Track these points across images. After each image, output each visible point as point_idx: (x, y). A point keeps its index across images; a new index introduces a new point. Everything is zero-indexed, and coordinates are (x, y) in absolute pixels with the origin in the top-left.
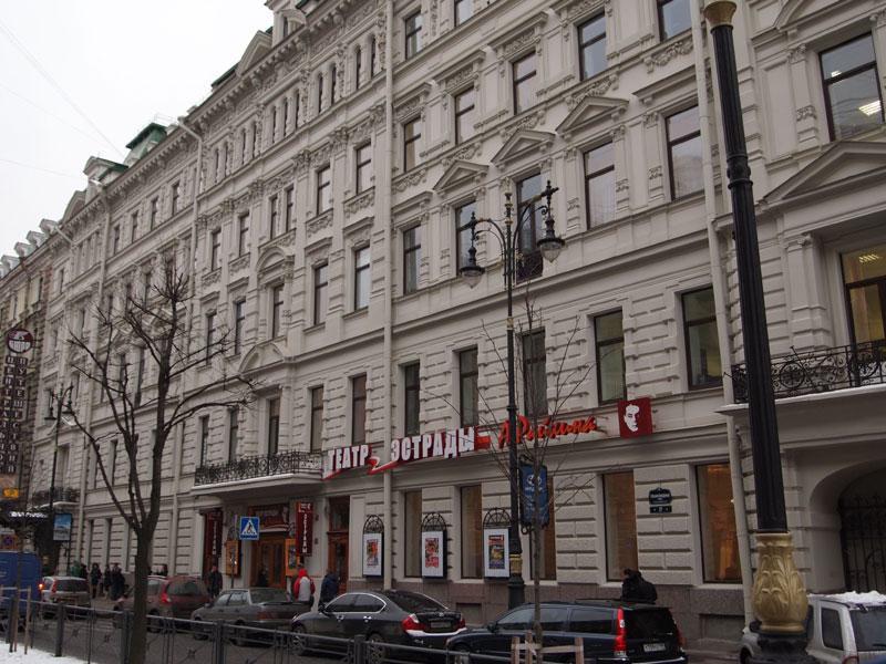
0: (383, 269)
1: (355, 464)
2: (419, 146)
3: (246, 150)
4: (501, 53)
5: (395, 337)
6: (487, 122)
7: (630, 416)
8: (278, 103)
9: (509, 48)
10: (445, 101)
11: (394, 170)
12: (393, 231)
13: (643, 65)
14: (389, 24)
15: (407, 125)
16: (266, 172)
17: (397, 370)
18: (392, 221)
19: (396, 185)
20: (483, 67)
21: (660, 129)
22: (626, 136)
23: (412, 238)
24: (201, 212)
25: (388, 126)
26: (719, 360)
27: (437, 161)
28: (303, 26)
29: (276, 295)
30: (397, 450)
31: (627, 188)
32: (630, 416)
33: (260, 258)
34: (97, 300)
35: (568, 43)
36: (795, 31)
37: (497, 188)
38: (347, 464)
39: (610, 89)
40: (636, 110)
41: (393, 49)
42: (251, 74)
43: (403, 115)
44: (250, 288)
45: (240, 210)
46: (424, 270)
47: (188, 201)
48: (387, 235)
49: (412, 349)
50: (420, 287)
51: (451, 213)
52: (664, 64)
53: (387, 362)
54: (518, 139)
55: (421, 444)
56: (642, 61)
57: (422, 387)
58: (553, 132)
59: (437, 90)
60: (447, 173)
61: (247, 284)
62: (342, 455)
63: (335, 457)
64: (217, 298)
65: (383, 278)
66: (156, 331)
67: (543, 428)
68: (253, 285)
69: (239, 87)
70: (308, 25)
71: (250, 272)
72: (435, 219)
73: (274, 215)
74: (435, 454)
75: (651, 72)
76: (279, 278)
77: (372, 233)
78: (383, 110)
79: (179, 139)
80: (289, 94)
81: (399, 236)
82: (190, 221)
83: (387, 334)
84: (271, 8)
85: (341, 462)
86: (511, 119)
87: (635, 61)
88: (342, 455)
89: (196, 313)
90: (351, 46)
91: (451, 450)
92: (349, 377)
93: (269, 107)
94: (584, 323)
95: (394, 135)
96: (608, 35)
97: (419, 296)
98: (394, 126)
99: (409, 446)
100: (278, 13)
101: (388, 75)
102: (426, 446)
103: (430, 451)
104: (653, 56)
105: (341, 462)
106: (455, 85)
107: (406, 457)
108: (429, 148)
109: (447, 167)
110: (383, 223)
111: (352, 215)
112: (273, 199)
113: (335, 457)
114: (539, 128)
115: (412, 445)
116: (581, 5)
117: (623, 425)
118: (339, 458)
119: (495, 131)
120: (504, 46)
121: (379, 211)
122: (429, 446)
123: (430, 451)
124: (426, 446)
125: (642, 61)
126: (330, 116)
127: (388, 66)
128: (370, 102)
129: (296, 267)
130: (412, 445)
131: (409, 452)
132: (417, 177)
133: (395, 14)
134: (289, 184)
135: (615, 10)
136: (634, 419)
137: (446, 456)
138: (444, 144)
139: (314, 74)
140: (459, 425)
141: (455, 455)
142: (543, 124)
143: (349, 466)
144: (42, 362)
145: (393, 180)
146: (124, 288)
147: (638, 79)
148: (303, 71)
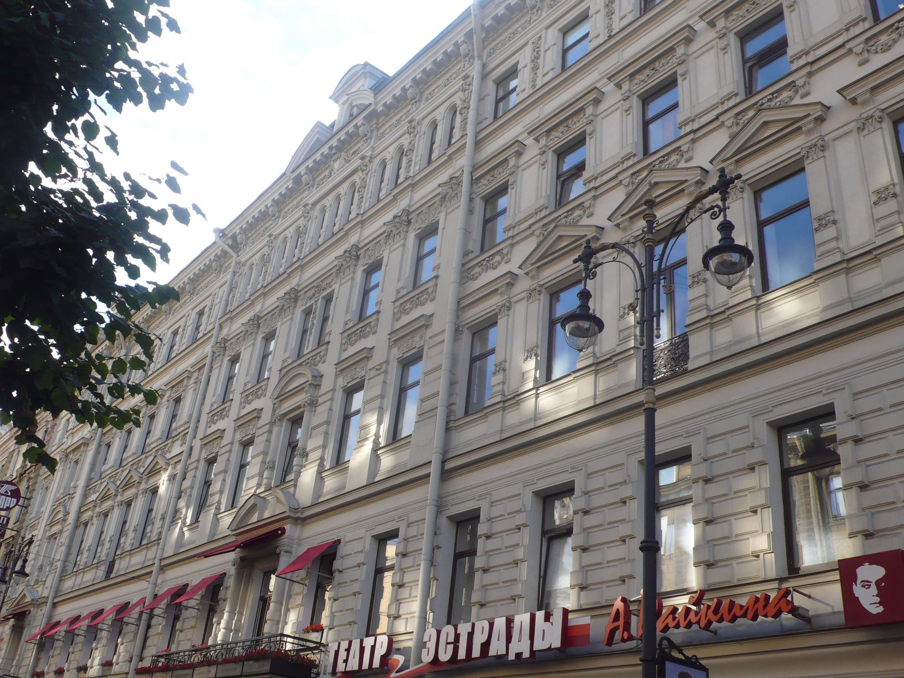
0: (440, 384)
1: (365, 666)
2: (502, 223)
3: (383, 185)
4: (543, 142)
5: (446, 475)
6: (816, 47)
7: (866, 584)
8: (329, 201)
9: (639, 77)
10: (544, 158)
11: (466, 253)
12: (457, 332)
13: (724, 129)
14: (475, 87)
15: (491, 199)
16: (266, 306)
17: (444, 522)
18: (458, 317)
19: (466, 272)
20: (521, 163)
21: (746, 201)
22: (827, 154)
23: (485, 340)
24: (221, 336)
25: (463, 200)
26: (20, 638)
27: (529, 232)
28: (370, 105)
29: (293, 432)
30: (432, 645)
31: (834, 222)
32: (866, 584)
33: (281, 379)
34: (93, 447)
35: (728, 56)
36: (626, 224)
37: (524, 302)
38: (353, 665)
39: (683, 161)
40: (844, 116)
41: (478, 113)
42: (302, 170)
43: (487, 186)
44: (262, 422)
45: (230, 353)
46: (499, 378)
47: (211, 327)
48: (447, 336)
49: (467, 492)
50: (488, 403)
51: (544, 298)
52: (887, 48)
53: (428, 513)
54: (761, 122)
55: (471, 635)
56: (723, 123)
57: (479, 551)
58: (707, 166)
59: (612, 96)
60: (628, 196)
61: (222, 437)
62: (348, 650)
63: (337, 652)
64: (258, 418)
65: (436, 394)
66: (147, 482)
67: (688, 610)
68: (266, 417)
69: (322, 154)
70: (376, 104)
71: (264, 403)
72: (520, 310)
73: (305, 332)
74: (492, 652)
75: (866, 62)
76: (299, 407)
77: (370, 367)
78: (459, 184)
79: (186, 280)
80: (344, 189)
81: (466, 337)
82: (208, 349)
83: (434, 470)
84: (337, 102)
85: (346, 661)
86: (639, 162)
87: (842, 51)
88: (348, 650)
89: (195, 457)
90: (426, 122)
91: (520, 646)
92: (536, 493)
93: (319, 206)
94: (766, 436)
95: (470, 211)
96: (680, 104)
97: (486, 416)
98: (471, 200)
99: (451, 639)
100: (344, 104)
101: (469, 141)
102: (479, 639)
103: (486, 646)
104: (868, 40)
105: (346, 661)
106: (561, 138)
107: (444, 657)
108: (811, 45)
109: (631, 188)
110: (443, 321)
111: (349, 347)
112: (308, 313)
113: (337, 652)
114: (585, 221)
115: (457, 636)
116: (746, 6)
117: (849, 598)
118: (342, 655)
119: (529, 232)
120: (632, 76)
121: (441, 308)
122: (484, 638)
123: (486, 646)
124: (479, 639)
125: (723, 123)
126: (391, 202)
127: (470, 131)
128: (443, 177)
129: (323, 390)
130: (457, 636)
131: (450, 648)
132: (498, 258)
133: (484, 77)
134: (329, 290)
135: (519, 181)
136: (874, 590)
137: (512, 657)
138: (855, 23)
139: (377, 161)
140: (535, 604)
141: (526, 654)
142: (591, 215)
143: (356, 668)
144: (25, 524)
145: (463, 265)
146: (172, 403)
147: (848, 71)
148: (363, 158)
